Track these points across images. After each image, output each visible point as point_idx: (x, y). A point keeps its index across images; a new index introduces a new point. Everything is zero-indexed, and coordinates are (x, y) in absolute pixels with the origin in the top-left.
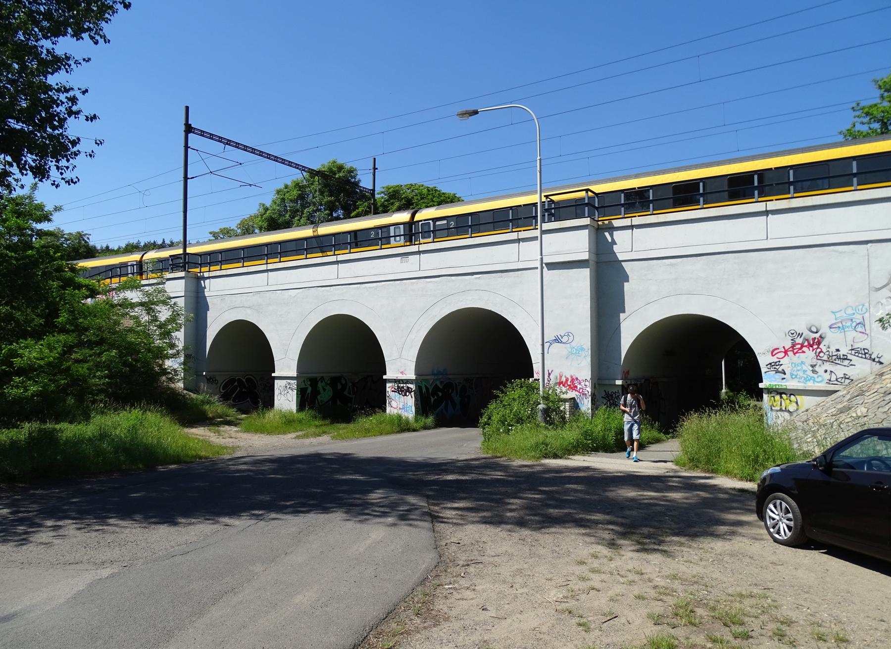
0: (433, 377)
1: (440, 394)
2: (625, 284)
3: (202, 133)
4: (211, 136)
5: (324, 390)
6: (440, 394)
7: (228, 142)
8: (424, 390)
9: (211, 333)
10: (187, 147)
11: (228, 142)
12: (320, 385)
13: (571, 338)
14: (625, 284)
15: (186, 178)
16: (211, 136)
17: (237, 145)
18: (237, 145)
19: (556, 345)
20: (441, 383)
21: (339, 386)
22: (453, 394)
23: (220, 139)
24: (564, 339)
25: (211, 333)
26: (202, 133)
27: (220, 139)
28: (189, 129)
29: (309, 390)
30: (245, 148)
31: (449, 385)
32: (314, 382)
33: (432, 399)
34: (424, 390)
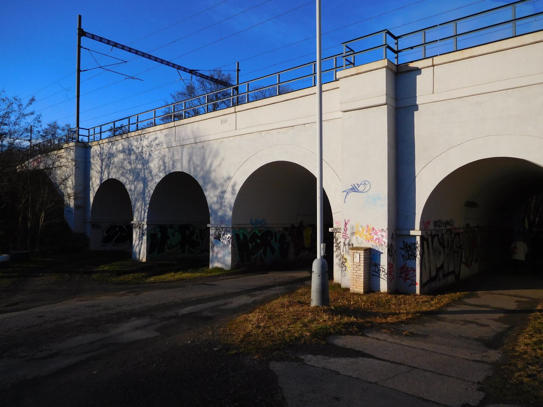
0: (251, 226)
1: (259, 241)
2: (415, 112)
3: (93, 37)
4: (101, 40)
5: (174, 235)
6: (259, 241)
7: (115, 45)
8: (241, 237)
9: (425, 184)
10: (79, 47)
11: (115, 45)
12: (169, 231)
13: (368, 187)
14: (415, 112)
15: (79, 71)
16: (101, 40)
17: (123, 47)
18: (123, 47)
19: (352, 194)
20: (260, 231)
21: (188, 233)
22: (273, 242)
23: (108, 42)
24: (361, 188)
25: (425, 184)
26: (93, 37)
27: (108, 42)
28: (82, 33)
29: (159, 236)
30: (130, 50)
31: (268, 234)
32: (163, 229)
33: (250, 246)
34: (241, 237)
